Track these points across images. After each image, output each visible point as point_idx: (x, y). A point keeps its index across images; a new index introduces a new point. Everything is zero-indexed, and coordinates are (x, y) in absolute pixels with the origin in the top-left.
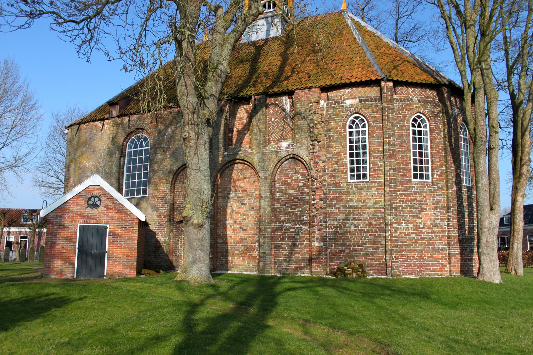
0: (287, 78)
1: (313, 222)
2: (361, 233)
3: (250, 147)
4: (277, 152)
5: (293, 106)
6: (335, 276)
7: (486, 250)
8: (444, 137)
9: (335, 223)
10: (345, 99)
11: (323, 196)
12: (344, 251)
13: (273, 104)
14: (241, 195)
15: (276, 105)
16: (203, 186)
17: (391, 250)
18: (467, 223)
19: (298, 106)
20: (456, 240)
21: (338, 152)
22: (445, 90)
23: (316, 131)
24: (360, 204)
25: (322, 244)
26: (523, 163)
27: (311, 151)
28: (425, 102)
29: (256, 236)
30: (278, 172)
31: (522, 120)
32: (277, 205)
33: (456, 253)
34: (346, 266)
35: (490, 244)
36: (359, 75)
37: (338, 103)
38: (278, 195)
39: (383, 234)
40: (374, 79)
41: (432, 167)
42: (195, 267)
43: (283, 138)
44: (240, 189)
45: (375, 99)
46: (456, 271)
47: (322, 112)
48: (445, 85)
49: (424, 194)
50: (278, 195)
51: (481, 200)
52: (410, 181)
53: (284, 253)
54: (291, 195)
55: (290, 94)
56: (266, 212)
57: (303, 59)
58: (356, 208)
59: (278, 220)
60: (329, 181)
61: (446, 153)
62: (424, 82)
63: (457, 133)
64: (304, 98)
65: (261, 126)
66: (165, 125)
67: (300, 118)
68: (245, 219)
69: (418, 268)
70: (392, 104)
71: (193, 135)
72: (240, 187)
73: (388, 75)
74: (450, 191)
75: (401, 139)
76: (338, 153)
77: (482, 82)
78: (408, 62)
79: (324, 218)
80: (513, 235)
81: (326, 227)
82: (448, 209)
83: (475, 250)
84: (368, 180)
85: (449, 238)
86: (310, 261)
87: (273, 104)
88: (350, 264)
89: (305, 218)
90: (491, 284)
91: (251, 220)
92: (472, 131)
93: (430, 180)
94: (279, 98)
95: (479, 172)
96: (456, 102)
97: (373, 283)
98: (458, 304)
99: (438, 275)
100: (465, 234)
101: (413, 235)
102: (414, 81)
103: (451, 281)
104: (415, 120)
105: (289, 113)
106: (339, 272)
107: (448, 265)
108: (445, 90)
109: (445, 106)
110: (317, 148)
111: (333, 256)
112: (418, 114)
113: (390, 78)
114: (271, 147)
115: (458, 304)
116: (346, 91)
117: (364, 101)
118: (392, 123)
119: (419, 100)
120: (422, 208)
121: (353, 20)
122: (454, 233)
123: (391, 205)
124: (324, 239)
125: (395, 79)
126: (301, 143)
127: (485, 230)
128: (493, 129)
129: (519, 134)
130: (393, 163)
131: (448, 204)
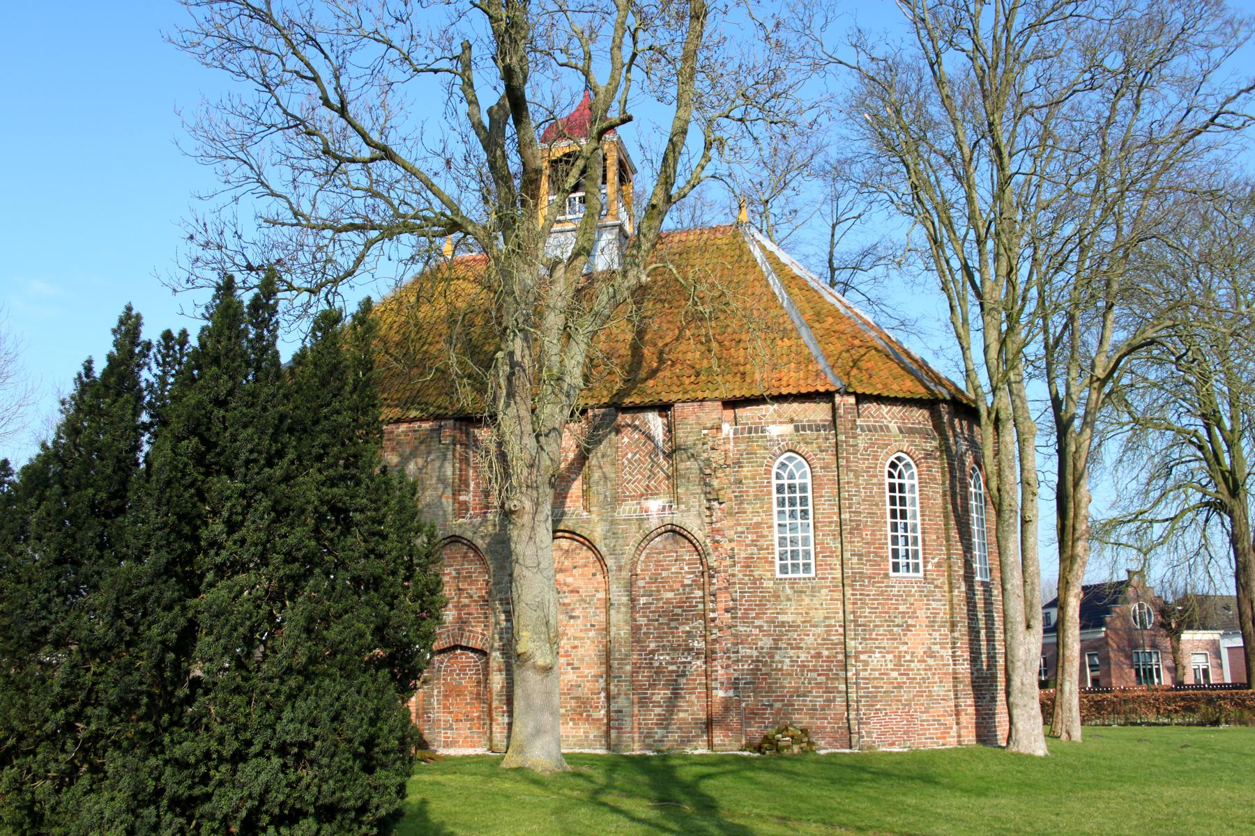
0: (653, 373)
1: (713, 652)
2: (802, 671)
3: (585, 508)
4: (641, 521)
5: (670, 431)
6: (759, 751)
7: (1022, 698)
8: (944, 495)
9: (755, 653)
10: (767, 423)
11: (731, 603)
12: (771, 706)
13: (629, 425)
14: (566, 601)
15: (636, 427)
16: (547, 597)
17: (857, 702)
18: (984, 649)
19: (680, 434)
20: (968, 681)
21: (757, 524)
22: (944, 408)
23: (715, 483)
24: (799, 620)
25: (731, 693)
26: (1077, 535)
27: (707, 520)
28: (911, 431)
29: (601, 680)
30: (643, 558)
31: (1074, 459)
32: (642, 621)
33: (968, 703)
34: (778, 732)
35: (1027, 689)
36: (794, 380)
37: (756, 431)
38: (643, 600)
39: (842, 674)
40: (822, 389)
41: (924, 549)
42: (539, 743)
43: (649, 493)
44: (565, 589)
45: (824, 426)
46: (970, 737)
47: (727, 446)
48: (945, 401)
49: (911, 600)
50: (643, 600)
51: (1011, 612)
52: (886, 576)
53: (658, 710)
54: (668, 601)
55: (663, 408)
56: (622, 633)
57: (677, 331)
58: (793, 626)
59: (643, 649)
60: (740, 576)
61: (946, 524)
62: (908, 396)
63: (965, 486)
64: (691, 420)
65: (608, 469)
66: (400, 456)
67: (684, 456)
68: (575, 647)
69: (905, 733)
70: (855, 437)
71: (528, 505)
72: (565, 584)
73: (845, 382)
74: (956, 592)
75: (869, 499)
76: (758, 525)
77: (1011, 408)
78: (876, 349)
79: (734, 644)
80: (1063, 667)
81: (738, 661)
82: (953, 625)
83: (1001, 696)
84: (812, 574)
85: (955, 678)
86: (709, 725)
87: (629, 425)
88: (787, 729)
89: (696, 644)
90: (1031, 757)
91: (589, 650)
92: (995, 491)
93: (921, 574)
94: (641, 415)
95: (1006, 564)
96: (962, 429)
97: (830, 760)
98: (987, 789)
99: (937, 743)
100: (981, 669)
101: (895, 674)
102: (892, 395)
103: (957, 756)
104: (893, 465)
105: (660, 444)
106: (766, 745)
107: (955, 726)
108: (944, 408)
109: (944, 437)
110: (717, 514)
111: (751, 715)
112: (900, 454)
113: (851, 390)
114: (627, 509)
115: (987, 789)
116: (770, 409)
117: (804, 428)
118: (855, 471)
119: (899, 428)
120: (908, 626)
121: (763, 248)
122: (964, 668)
123: (855, 621)
124: (734, 684)
125: (860, 391)
126: (687, 504)
127: (1019, 664)
128: (1029, 489)
129: (1070, 478)
130: (858, 545)
131: (952, 617)
